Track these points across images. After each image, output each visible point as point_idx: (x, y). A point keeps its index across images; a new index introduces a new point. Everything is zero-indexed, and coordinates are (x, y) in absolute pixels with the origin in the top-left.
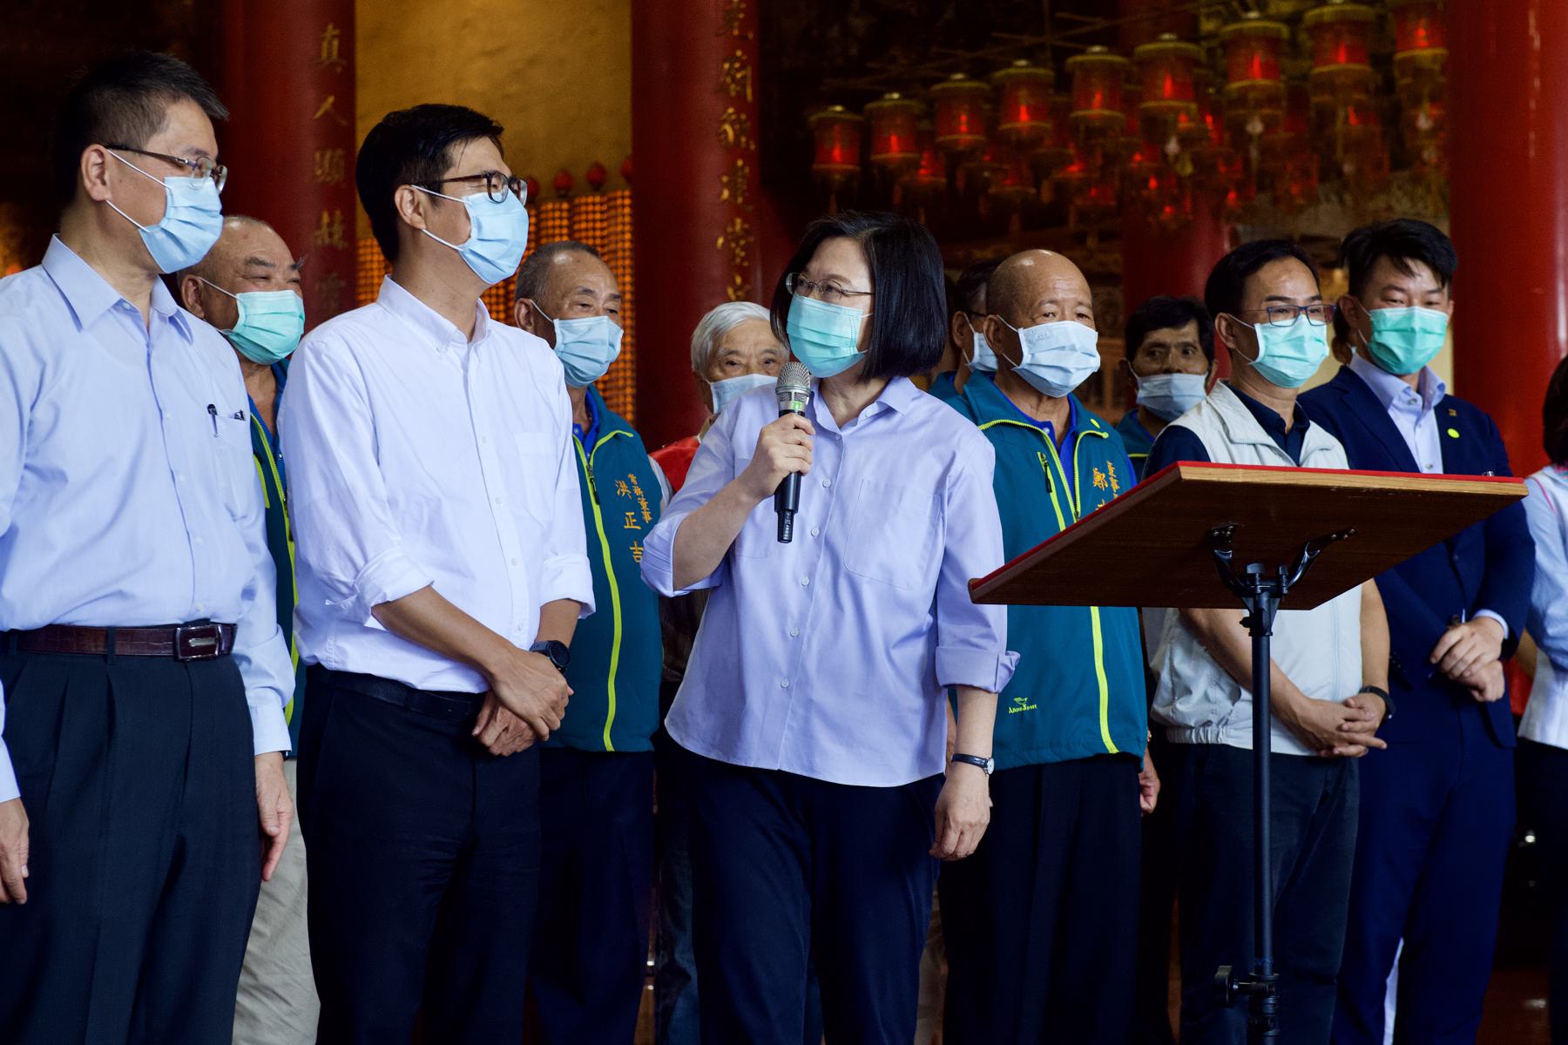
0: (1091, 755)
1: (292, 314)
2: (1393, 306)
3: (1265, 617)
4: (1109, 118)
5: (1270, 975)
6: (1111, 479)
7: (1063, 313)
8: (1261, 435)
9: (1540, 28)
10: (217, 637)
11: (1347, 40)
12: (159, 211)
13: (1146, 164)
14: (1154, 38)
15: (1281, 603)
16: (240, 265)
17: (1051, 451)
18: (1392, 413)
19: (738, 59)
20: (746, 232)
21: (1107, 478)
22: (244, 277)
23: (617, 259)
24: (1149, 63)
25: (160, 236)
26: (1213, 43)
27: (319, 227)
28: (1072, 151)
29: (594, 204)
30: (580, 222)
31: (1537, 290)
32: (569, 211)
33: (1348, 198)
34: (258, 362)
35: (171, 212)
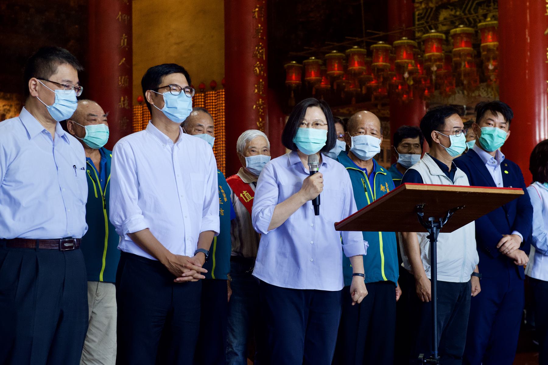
0: (378, 281)
1: (104, 132)
2: (489, 126)
3: (435, 235)
4: (385, 65)
5: (437, 357)
6: (387, 188)
7: (366, 132)
8: (440, 172)
9: (530, 35)
10: (74, 243)
11: (465, 39)
12: (53, 102)
13: (397, 81)
14: (400, 38)
15: (440, 230)
16: (86, 116)
17: (366, 178)
18: (487, 165)
19: (261, 46)
20: (263, 104)
21: (385, 188)
22: (87, 120)
23: (220, 112)
24: (399, 47)
25: (53, 109)
26: (420, 40)
27: (120, 102)
28: (372, 76)
29: (212, 94)
30: (208, 100)
31: (529, 123)
32: (204, 96)
33: (465, 92)
34: (94, 148)
35: (56, 101)
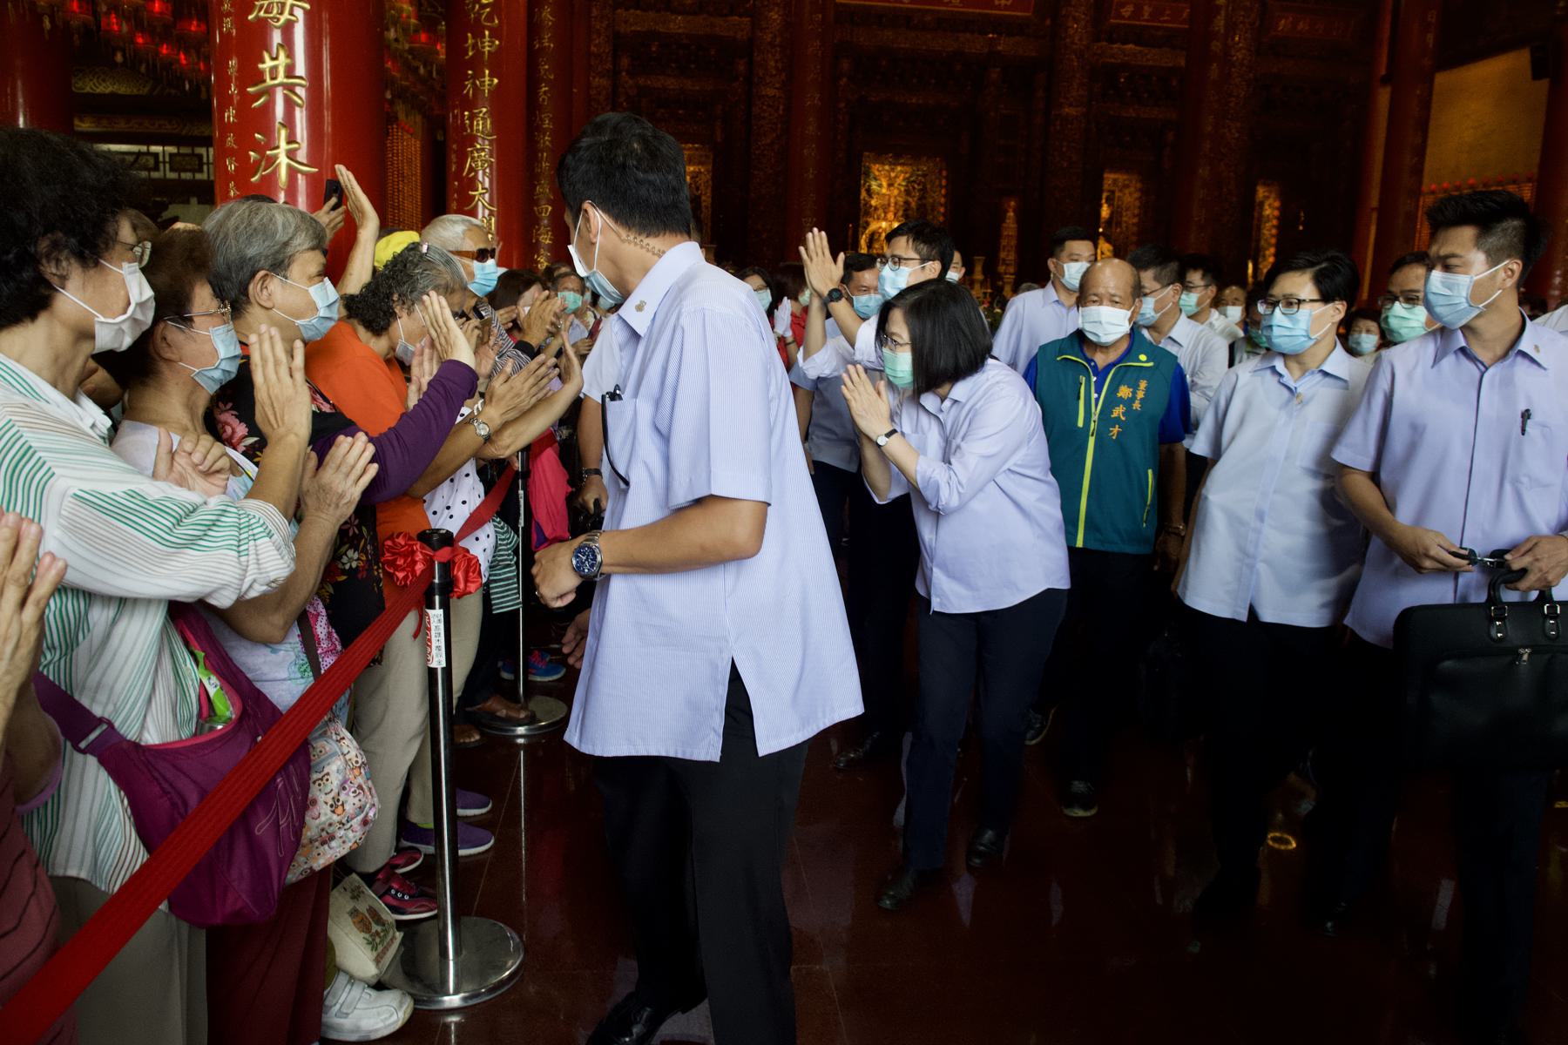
31: (1522, 289)
